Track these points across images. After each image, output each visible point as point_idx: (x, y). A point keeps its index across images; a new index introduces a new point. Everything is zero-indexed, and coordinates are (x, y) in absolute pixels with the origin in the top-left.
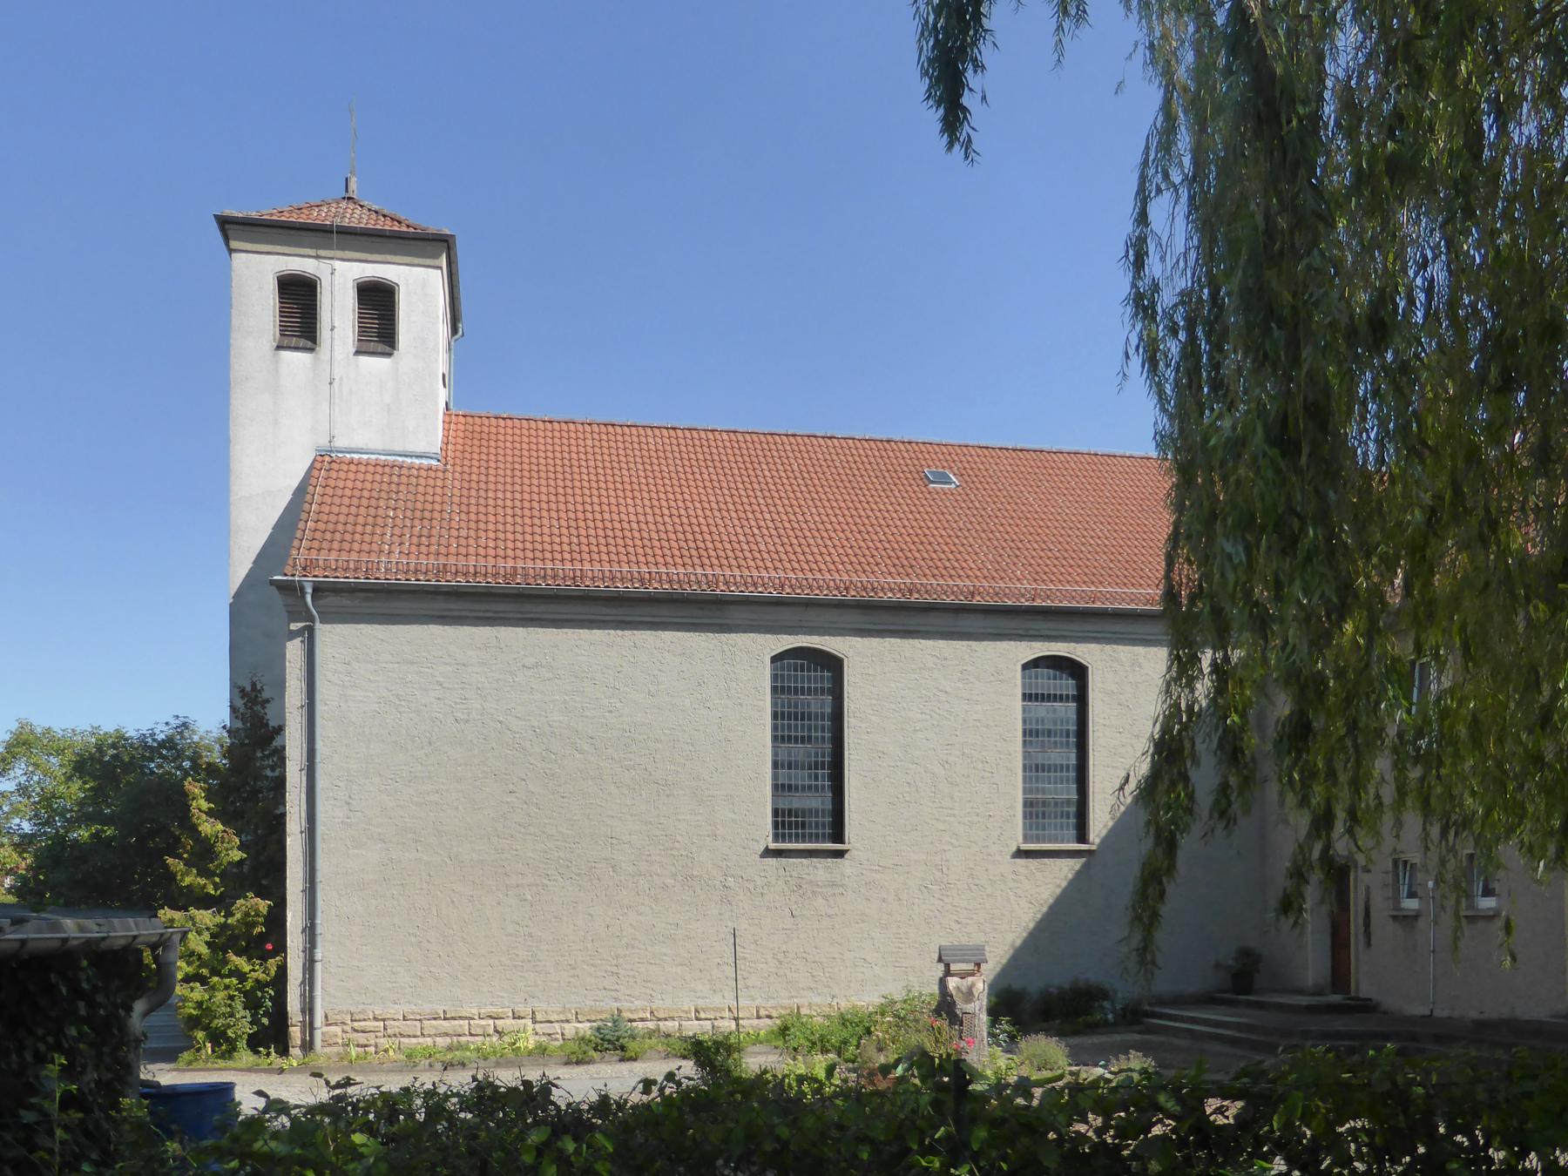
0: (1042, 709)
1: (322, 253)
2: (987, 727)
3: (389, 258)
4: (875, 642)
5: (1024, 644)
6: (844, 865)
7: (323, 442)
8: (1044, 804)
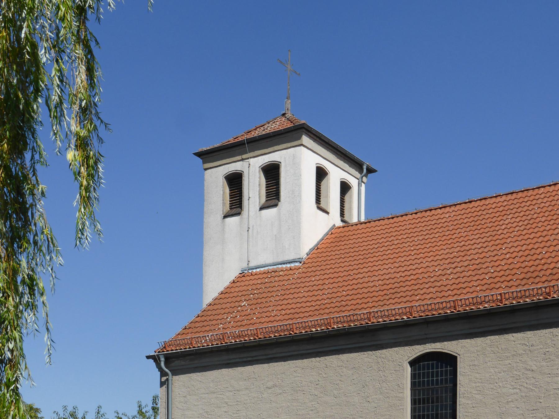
1: (244, 156)
3: (276, 148)
4: (479, 341)
7: (245, 265)
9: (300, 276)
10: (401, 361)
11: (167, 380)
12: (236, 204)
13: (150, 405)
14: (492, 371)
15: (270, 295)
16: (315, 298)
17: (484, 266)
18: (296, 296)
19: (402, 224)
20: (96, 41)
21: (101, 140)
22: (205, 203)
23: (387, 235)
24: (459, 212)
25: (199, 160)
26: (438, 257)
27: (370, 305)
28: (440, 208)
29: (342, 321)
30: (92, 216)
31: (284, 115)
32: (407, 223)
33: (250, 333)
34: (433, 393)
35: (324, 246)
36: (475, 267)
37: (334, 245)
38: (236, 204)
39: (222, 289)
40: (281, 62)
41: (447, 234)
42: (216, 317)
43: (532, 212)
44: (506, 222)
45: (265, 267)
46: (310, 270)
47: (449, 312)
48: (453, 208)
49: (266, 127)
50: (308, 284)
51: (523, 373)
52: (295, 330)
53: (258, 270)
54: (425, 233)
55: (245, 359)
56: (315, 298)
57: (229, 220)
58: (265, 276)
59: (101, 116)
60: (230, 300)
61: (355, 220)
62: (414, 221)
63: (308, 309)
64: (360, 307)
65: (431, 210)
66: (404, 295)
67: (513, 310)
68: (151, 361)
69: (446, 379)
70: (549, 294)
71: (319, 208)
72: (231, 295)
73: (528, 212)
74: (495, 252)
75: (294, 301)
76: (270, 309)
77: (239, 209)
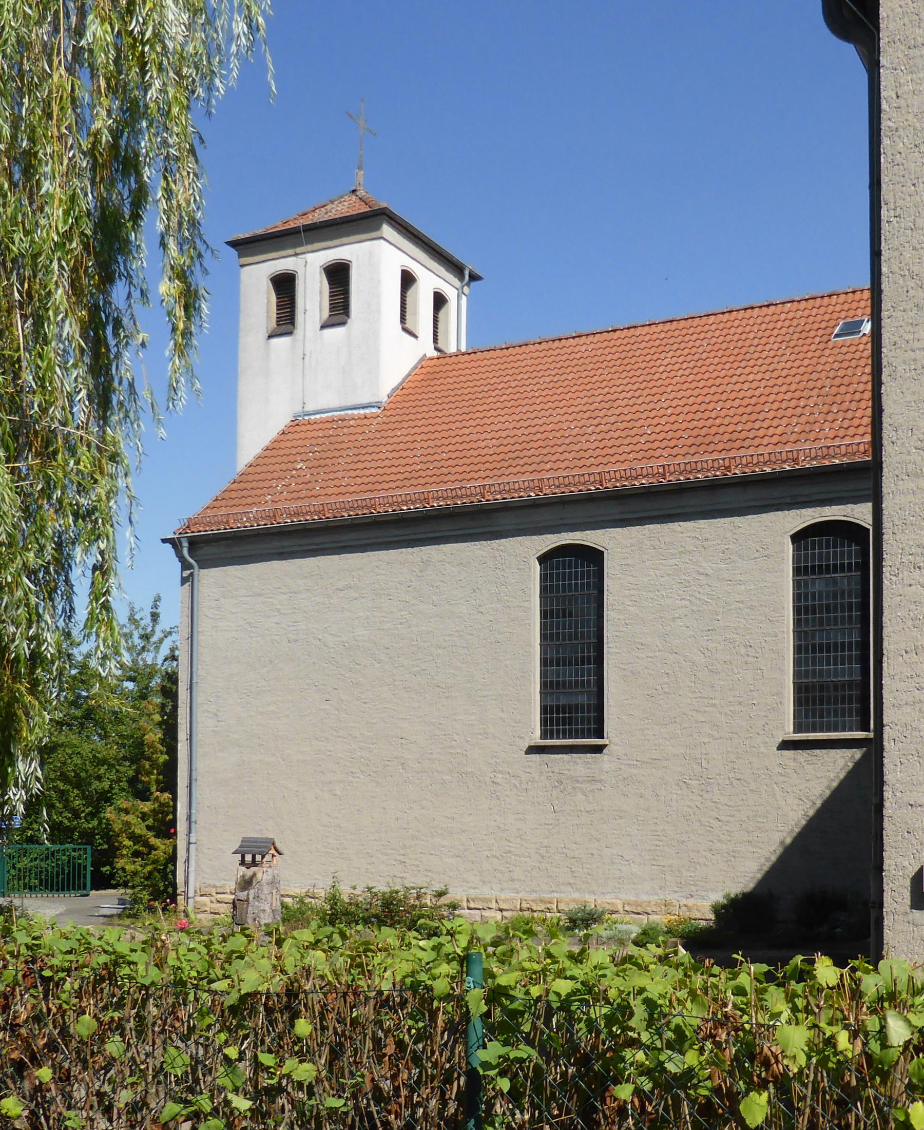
0: (818, 585)
1: (298, 250)
2: (751, 608)
5: (794, 513)
6: (602, 759)
7: (298, 409)
8: (822, 688)
9: (380, 427)
10: (525, 555)
11: (192, 574)
12: (286, 318)
13: (148, 611)
14: (652, 573)
15: (337, 454)
16: (403, 462)
17: (638, 424)
18: (374, 456)
19: (522, 358)
20: (201, 138)
21: (205, 271)
22: (242, 316)
23: (500, 372)
24: (599, 345)
25: (233, 252)
26: (572, 409)
27: (482, 474)
28: (573, 338)
29: (445, 496)
30: (190, 371)
31: (354, 191)
32: (528, 357)
33: (312, 510)
34: (570, 604)
35: (412, 385)
36: (625, 425)
37: (425, 384)
38: (286, 318)
39: (266, 443)
40: (351, 116)
41: (584, 375)
42: (261, 484)
43: (700, 350)
44: (665, 362)
45: (328, 412)
46: (393, 419)
47: (593, 488)
48: (591, 338)
49: (328, 207)
50: (391, 441)
51: (694, 579)
52: (378, 507)
53: (318, 416)
54: (553, 373)
55: (306, 548)
56: (403, 462)
57: (275, 341)
58: (328, 425)
59: (204, 237)
60: (278, 460)
61: (452, 349)
62: (537, 354)
63: (393, 477)
64: (468, 477)
65: (560, 340)
66: (529, 461)
67: (680, 490)
68: (169, 546)
69: (589, 583)
70: (728, 468)
71: (405, 330)
72: (281, 452)
73: (694, 350)
74: (652, 405)
75: (374, 464)
76: (340, 475)
77: (290, 326)
